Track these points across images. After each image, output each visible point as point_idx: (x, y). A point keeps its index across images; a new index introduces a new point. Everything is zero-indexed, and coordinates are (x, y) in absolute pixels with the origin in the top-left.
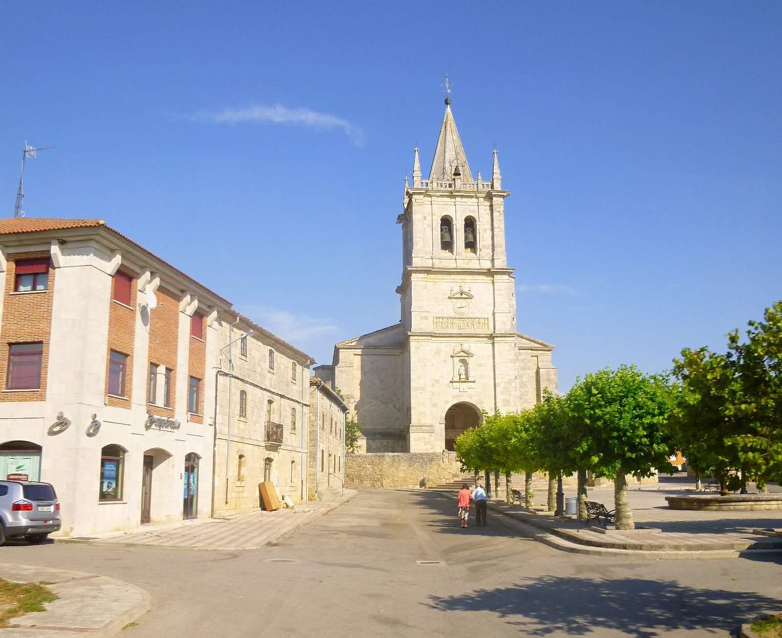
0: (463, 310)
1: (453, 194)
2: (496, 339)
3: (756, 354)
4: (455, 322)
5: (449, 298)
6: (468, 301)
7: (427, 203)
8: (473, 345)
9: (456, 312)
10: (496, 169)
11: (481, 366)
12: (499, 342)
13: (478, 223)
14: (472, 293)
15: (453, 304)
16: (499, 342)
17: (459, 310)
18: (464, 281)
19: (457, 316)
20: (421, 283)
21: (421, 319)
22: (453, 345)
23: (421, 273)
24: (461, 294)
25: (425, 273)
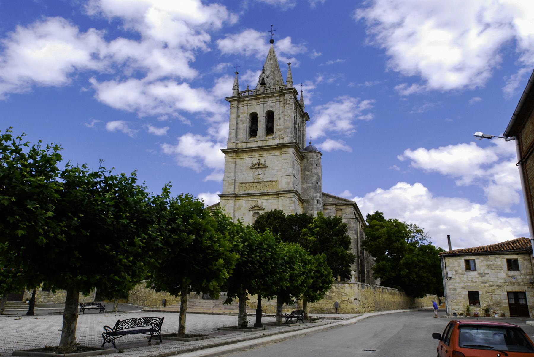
0: (260, 176)
6: (264, 169)
8: (264, 201)
9: (254, 178)
14: (267, 164)
15: (253, 172)
17: (256, 177)
18: (261, 156)
19: (255, 181)
21: (229, 185)
22: (250, 202)
23: (231, 153)
24: (259, 165)
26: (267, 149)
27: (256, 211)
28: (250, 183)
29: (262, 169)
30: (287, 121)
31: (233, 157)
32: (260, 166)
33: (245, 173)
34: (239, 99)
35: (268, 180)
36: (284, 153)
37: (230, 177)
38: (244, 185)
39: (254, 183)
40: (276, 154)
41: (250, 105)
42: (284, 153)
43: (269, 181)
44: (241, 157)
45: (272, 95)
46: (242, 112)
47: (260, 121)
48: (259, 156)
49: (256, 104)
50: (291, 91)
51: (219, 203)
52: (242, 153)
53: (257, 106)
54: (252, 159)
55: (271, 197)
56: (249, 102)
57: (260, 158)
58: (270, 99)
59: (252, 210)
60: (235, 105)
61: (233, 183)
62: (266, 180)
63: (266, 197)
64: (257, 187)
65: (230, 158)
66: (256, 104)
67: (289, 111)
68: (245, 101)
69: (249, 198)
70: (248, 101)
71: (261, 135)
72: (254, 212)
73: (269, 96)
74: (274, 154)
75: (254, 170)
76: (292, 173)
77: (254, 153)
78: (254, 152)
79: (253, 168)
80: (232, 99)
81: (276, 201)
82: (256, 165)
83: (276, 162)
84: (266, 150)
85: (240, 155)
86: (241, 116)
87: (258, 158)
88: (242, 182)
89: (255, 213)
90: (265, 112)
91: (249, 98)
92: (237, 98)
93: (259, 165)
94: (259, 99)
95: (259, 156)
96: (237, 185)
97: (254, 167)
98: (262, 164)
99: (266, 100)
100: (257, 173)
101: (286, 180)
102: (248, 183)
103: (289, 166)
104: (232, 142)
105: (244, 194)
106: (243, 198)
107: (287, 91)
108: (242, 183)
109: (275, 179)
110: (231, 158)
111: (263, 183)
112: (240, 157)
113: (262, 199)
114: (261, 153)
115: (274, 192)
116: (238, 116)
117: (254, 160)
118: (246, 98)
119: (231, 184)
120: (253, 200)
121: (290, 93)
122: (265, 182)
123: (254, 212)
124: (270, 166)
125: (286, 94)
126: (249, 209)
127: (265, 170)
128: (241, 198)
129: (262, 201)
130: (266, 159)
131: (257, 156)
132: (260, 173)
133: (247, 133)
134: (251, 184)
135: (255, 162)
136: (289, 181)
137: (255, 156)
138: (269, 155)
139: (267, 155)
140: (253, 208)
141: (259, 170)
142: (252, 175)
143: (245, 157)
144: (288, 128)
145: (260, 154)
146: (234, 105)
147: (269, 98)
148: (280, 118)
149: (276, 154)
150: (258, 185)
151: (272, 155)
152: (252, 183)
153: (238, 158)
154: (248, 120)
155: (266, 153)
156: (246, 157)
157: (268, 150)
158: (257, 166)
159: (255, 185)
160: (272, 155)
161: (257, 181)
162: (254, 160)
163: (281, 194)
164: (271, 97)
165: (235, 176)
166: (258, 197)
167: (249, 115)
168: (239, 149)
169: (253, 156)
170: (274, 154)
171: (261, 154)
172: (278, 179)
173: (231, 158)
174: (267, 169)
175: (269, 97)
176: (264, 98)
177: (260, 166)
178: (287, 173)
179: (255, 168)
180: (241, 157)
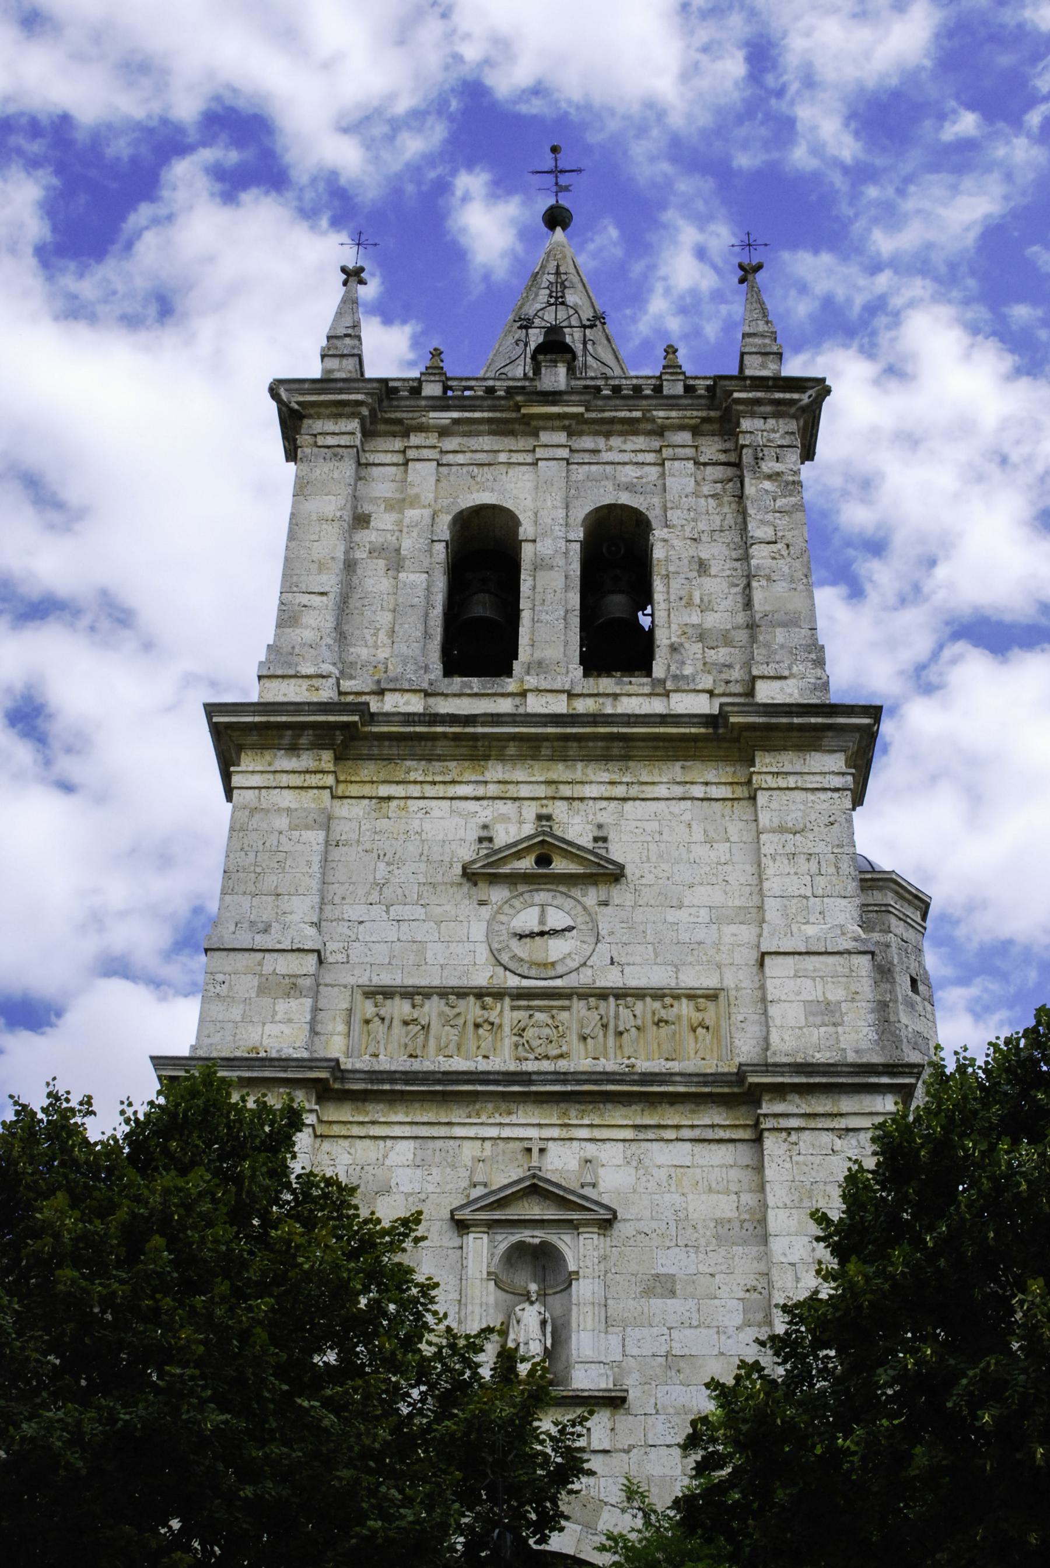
0: (556, 948)
1: (524, 411)
2: (625, 967)
3: (1022, 1043)
4: (493, 1016)
5: (470, 876)
6: (591, 896)
7: (388, 458)
8: (610, 1154)
9: (505, 958)
10: (702, 730)
11: (673, 1293)
12: (794, 1123)
13: (658, 533)
14: (617, 852)
15: (485, 912)
16: (794, 1123)
17: (521, 949)
18: (566, 791)
19: (513, 981)
20: (287, 799)
21: (262, 990)
22: (470, 1150)
23: (293, 749)
24: (544, 860)
25: (318, 745)
26: (617, 749)
27: (533, 1237)
28: (462, 993)
29: (576, 892)
30: (769, 579)
31: (313, 780)
32: (560, 865)
33: (419, 912)
34: (373, 412)
35: (636, 979)
36: (771, 782)
37: (276, 927)
38: (401, 1008)
39: (499, 995)
40: (698, 791)
41: (460, 458)
42: (771, 782)
43: (640, 994)
44: (384, 791)
45: (638, 414)
46: (389, 495)
47: (540, 565)
48: (541, 791)
49: (503, 457)
50: (796, 396)
51: (802, 463)
52: (389, 759)
53: (514, 471)
54: (485, 812)
55: (672, 1116)
56: (451, 443)
57: (559, 810)
58: (616, 441)
59: (492, 1225)
60: (344, 440)
61: (308, 982)
62: (611, 979)
63: (619, 1115)
64: (529, 1033)
65: (285, 780)
66: (503, 457)
67: (782, 522)
68: (422, 428)
69: (457, 1114)
70: (444, 432)
71: (552, 653)
72: (505, 1240)
73: (612, 421)
74: (678, 791)
75: (498, 894)
76: (864, 941)
77: (496, 771)
78: (501, 758)
79: (494, 879)
80: (322, 398)
81: (722, 1154)
82: (519, 855)
83: (700, 851)
84: (606, 758)
85: (368, 770)
86: (383, 521)
87: (531, 811)
88: (385, 979)
89: (518, 1254)
90: (582, 510)
91: (455, 415)
92: (360, 397)
93: (544, 860)
94: (530, 427)
95: (541, 791)
96: (337, 1001)
97: (505, 870)
98: (571, 850)
99: (587, 442)
100: (528, 919)
101: (811, 991)
102: (444, 993)
103: (821, 881)
104: (311, 671)
105: (409, 1077)
106: (399, 1116)
107: (759, 395)
108: (387, 993)
109: (692, 978)
110: (296, 780)
111: (578, 1006)
112: (367, 790)
113: (584, 1133)
114: (559, 771)
115: (705, 1078)
116: (361, 520)
117: (505, 819)
118: (432, 415)
119: (292, 988)
120: (493, 1132)
121: (777, 415)
122: (603, 995)
123: (505, 1240)
124: (649, 879)
125: (753, 415)
126: (465, 1215)
127: (605, 903)
128: (377, 1111)
129: (591, 1149)
130: (604, 818)
131: (525, 791)
132: (556, 919)
133: (427, 635)
134: (471, 1009)
135: (505, 835)
136: (836, 994)
137: (512, 791)
138: (634, 791)
139: (620, 791)
140: (501, 1203)
141: (542, 897)
142: (478, 931)
143: (415, 790)
144: (784, 625)
145: (553, 776)
146: (330, 441)
147: (607, 435)
148: (702, 567)
149: (698, 791)
150: (540, 1016)
151: (662, 791)
152: (480, 994)
153: (354, 790)
154: (440, 547)
155: (606, 777)
156: (430, 791)
157: (626, 758)
158: (527, 864)
159: (507, 1015)
160: (662, 791)
161: (526, 983)
162: (505, 819)
163: (780, 1091)
164: (630, 428)
165: (317, 925)
166: (551, 1115)
167: (445, 520)
168: (372, 718)
169: (492, 790)
170: (678, 791)
171: (567, 776)
172: (729, 982)
173: (296, 780)
174: (618, 894)
175: (607, 428)
176: (574, 426)
177: (560, 865)
178: (810, 930)
179: (514, 879)
180: (384, 791)
